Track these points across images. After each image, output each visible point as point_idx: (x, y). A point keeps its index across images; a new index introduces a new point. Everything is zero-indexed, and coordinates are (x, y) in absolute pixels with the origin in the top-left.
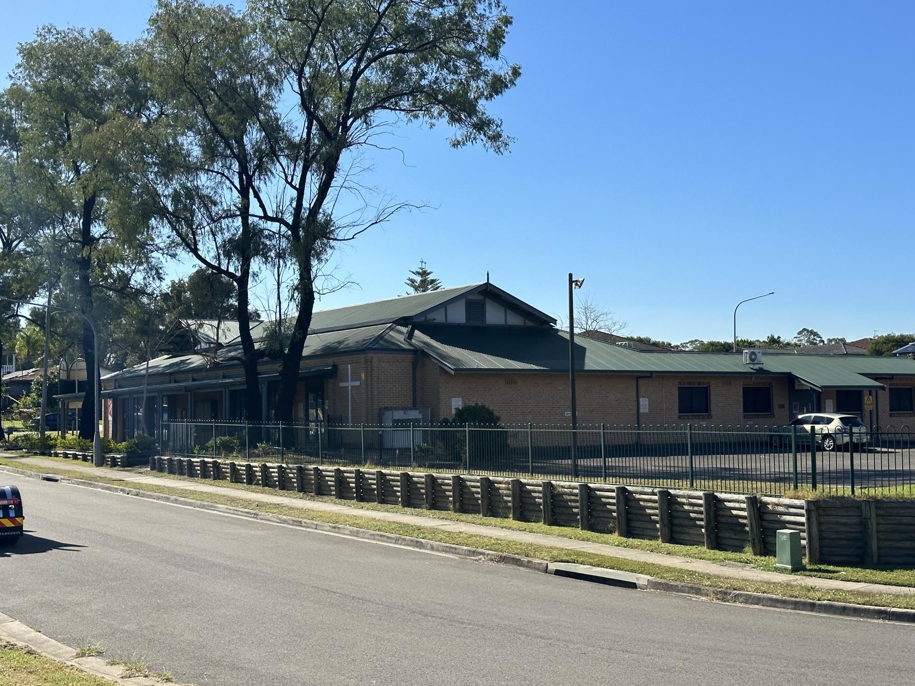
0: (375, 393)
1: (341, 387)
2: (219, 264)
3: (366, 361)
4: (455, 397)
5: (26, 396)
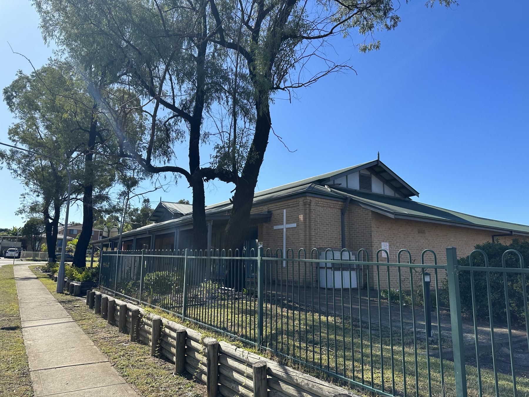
0: (313, 234)
1: (275, 230)
2: (174, 102)
3: (305, 204)
4: (383, 241)
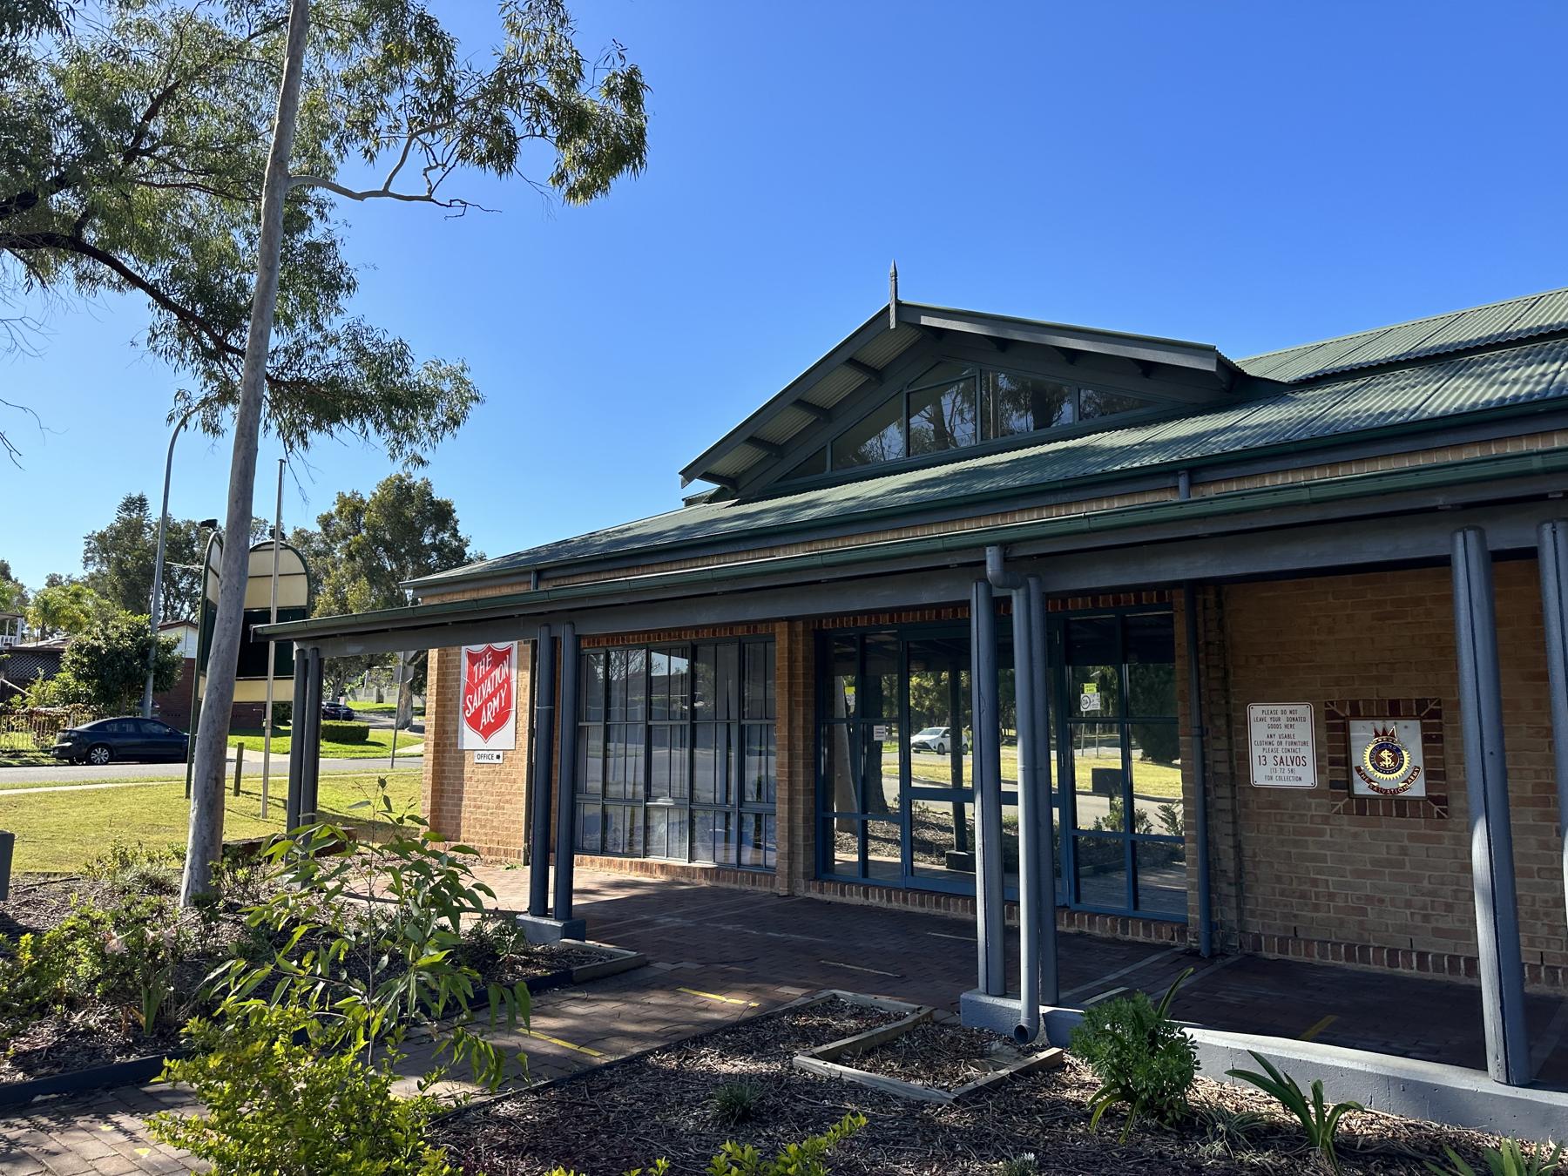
5: (44, 680)
